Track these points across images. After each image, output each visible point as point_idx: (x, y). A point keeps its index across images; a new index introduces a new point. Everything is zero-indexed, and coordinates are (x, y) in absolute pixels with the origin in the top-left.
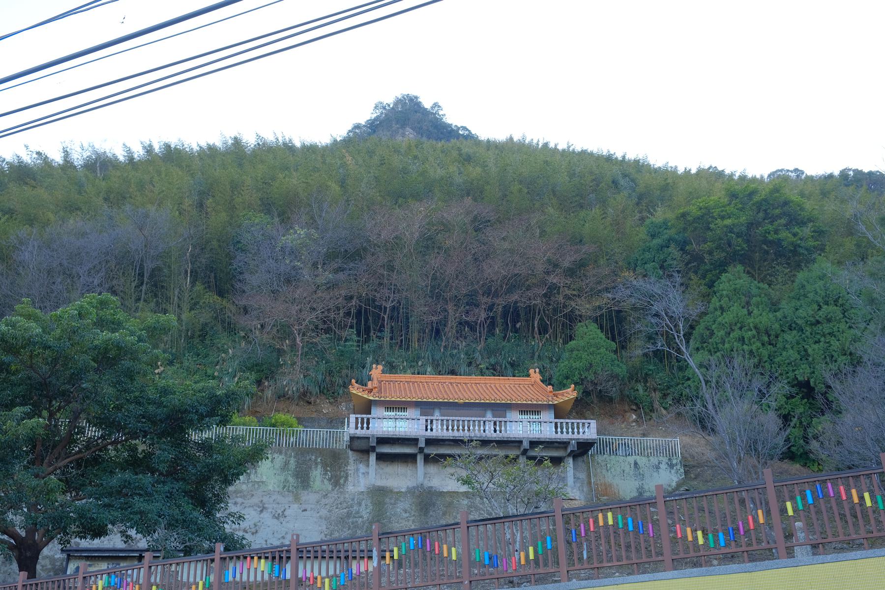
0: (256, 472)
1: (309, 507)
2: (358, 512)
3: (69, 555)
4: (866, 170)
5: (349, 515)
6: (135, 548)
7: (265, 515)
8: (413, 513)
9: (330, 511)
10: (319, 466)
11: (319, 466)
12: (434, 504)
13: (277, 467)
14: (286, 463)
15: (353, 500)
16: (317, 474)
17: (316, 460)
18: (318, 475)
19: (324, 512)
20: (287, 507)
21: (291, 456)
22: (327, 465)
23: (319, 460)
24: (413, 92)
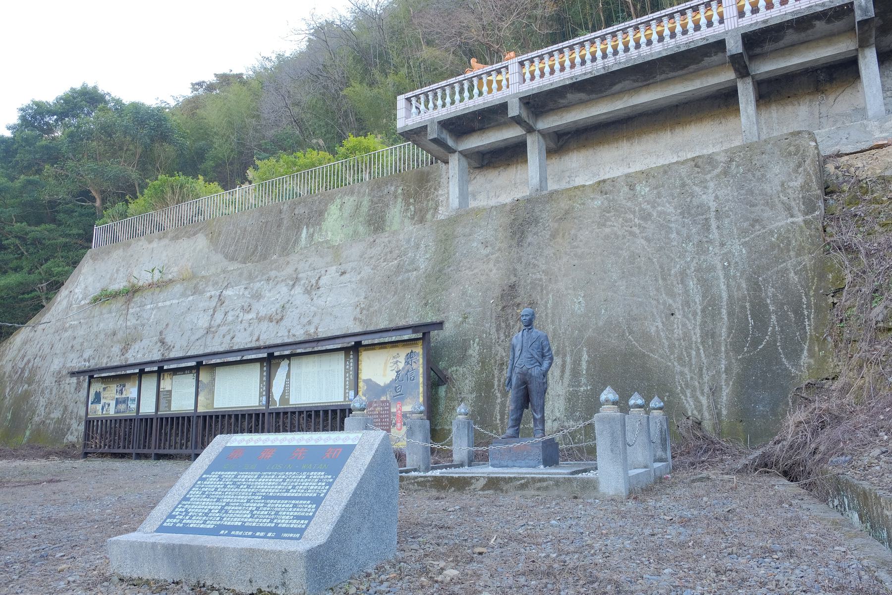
0: (320, 229)
1: (347, 267)
2: (412, 262)
3: (91, 377)
4: (127, 100)
5: (399, 269)
6: (131, 361)
7: (298, 290)
8: (498, 245)
9: (375, 268)
10: (400, 200)
11: (400, 200)
12: (536, 221)
13: (346, 215)
14: (358, 207)
15: (408, 241)
16: (396, 213)
17: (396, 191)
18: (398, 214)
19: (367, 271)
20: (323, 272)
21: (364, 195)
22: (409, 197)
23: (400, 191)
24: (26, 101)
